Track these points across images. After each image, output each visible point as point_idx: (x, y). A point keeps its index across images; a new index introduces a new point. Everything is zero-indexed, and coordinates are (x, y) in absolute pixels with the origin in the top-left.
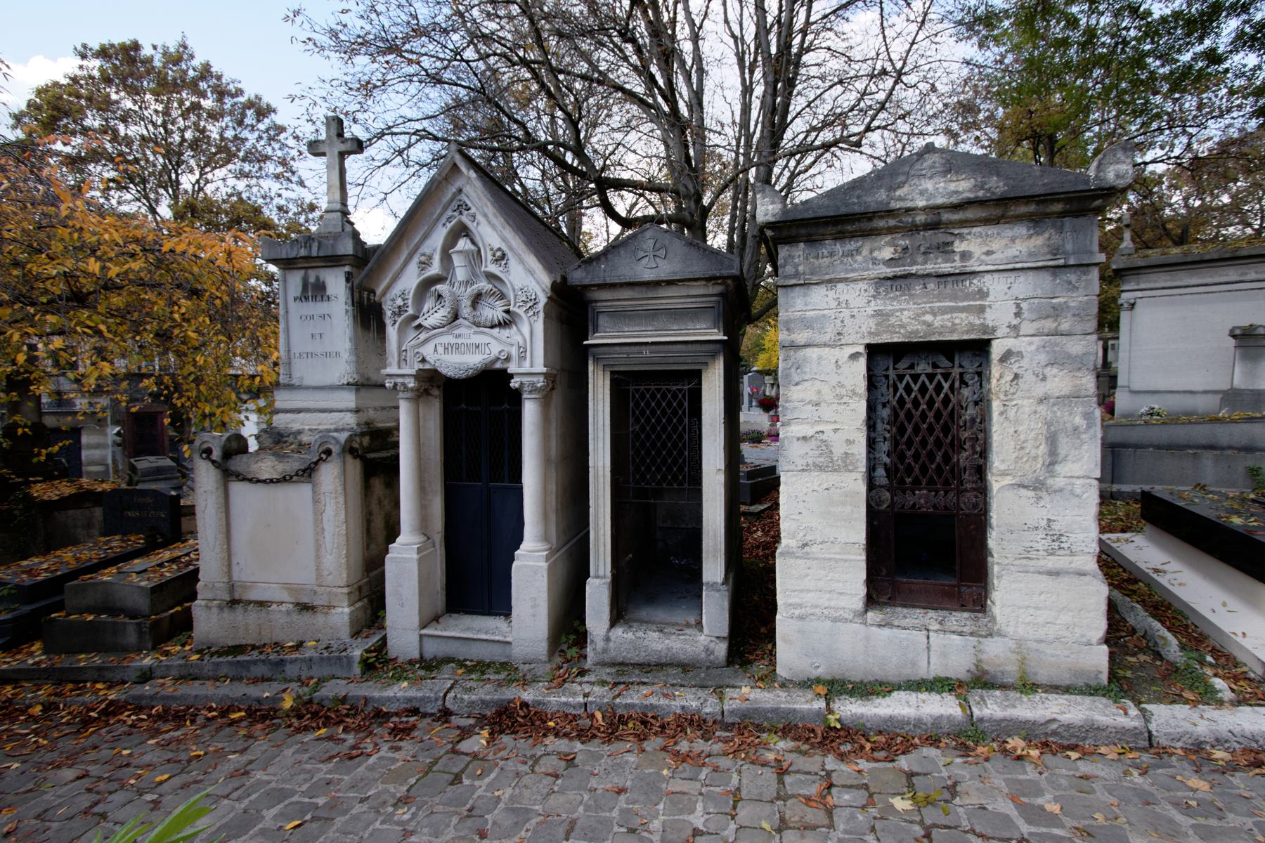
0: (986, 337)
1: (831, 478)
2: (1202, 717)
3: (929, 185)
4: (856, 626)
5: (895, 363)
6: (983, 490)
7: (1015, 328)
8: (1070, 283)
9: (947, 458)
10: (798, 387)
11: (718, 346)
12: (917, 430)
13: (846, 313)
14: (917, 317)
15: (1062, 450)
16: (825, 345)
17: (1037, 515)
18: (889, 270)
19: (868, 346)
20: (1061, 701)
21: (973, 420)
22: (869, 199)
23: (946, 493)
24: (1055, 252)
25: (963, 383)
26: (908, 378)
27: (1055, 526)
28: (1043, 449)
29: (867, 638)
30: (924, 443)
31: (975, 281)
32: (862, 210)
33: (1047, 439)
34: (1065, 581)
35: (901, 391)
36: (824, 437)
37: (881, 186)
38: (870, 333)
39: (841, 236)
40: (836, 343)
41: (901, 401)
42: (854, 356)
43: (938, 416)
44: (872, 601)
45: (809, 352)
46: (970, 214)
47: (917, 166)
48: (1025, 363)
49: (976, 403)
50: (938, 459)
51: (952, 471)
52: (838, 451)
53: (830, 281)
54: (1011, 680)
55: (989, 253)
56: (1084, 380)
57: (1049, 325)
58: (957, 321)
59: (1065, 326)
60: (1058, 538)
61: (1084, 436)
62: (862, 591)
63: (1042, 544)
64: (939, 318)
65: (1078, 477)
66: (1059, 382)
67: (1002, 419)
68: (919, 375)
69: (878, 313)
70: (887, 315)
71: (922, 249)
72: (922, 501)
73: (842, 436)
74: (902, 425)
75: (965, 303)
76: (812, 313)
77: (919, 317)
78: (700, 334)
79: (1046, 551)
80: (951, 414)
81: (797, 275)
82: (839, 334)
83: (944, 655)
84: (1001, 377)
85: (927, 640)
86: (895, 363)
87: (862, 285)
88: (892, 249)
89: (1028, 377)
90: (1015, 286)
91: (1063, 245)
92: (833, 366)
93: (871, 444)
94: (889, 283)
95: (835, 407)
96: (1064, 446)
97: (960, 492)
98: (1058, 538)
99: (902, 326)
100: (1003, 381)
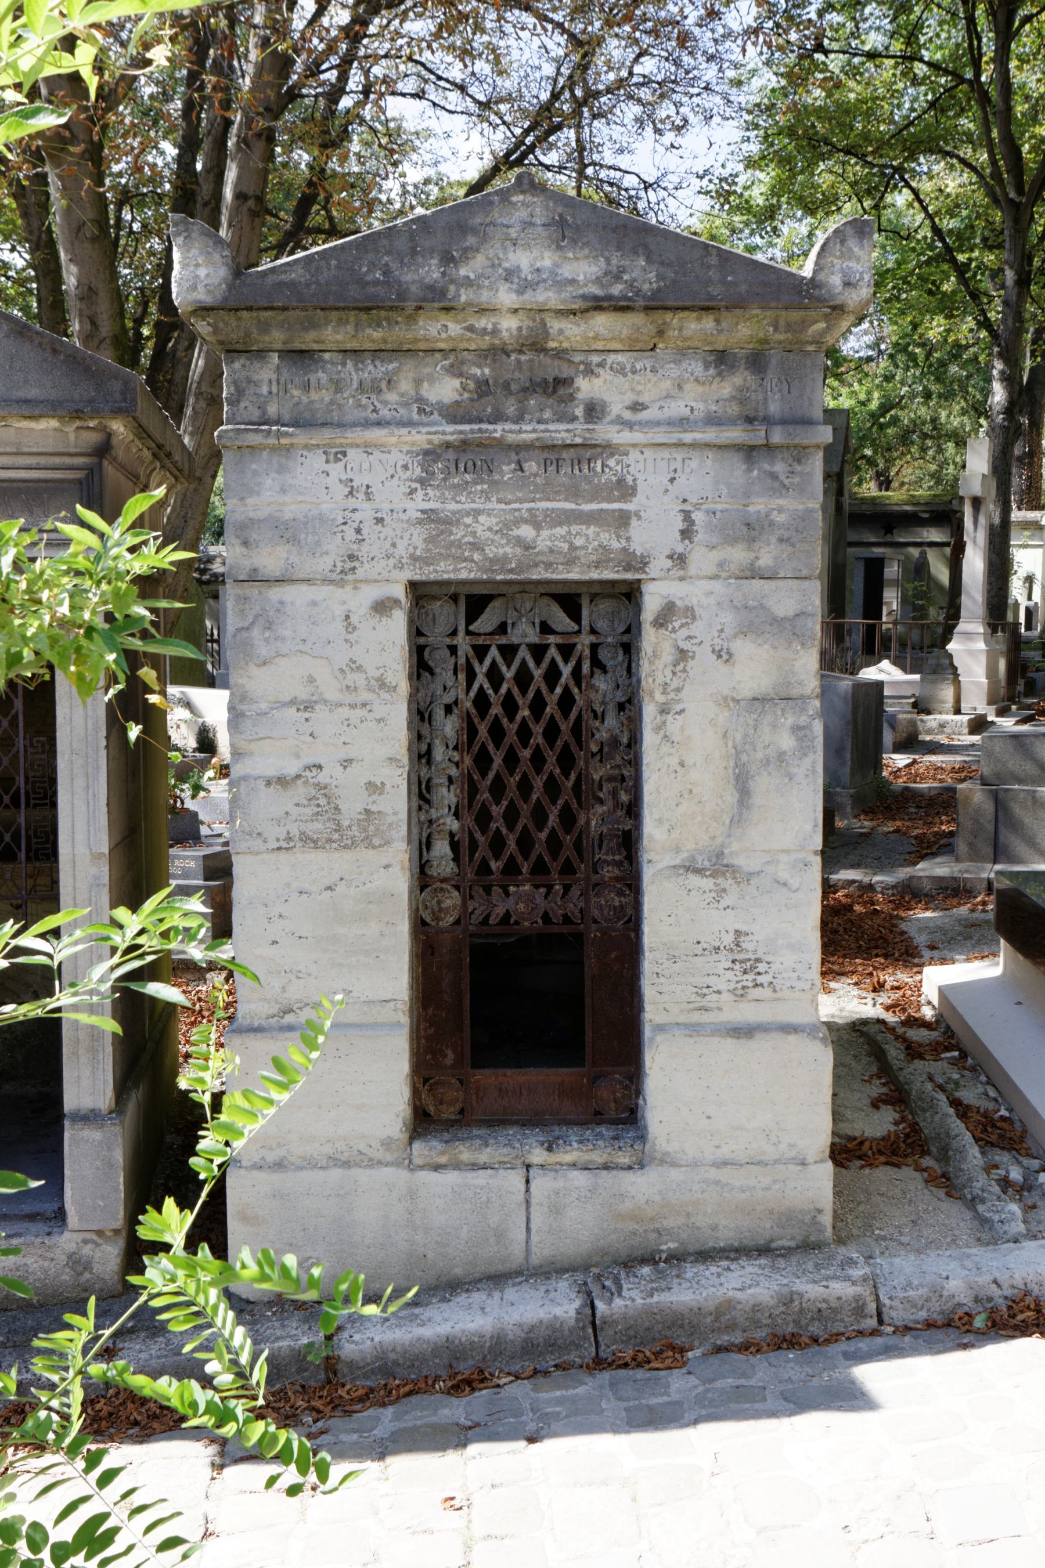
0: (629, 576)
4: (401, 1176)
6: (631, 884)
7: (680, 560)
8: (774, 476)
9: (568, 818)
12: (511, 760)
14: (505, 527)
17: (718, 924)
19: (413, 586)
20: (750, 1269)
21: (615, 742)
25: (597, 664)
26: (494, 653)
29: (412, 1194)
31: (611, 462)
34: (761, 1044)
35: (481, 680)
36: (323, 777)
40: (345, 574)
41: (482, 702)
42: (382, 607)
43: (552, 732)
44: (423, 1121)
48: (697, 629)
49: (621, 707)
50: (553, 820)
51: (578, 846)
52: (352, 806)
57: (738, 555)
58: (579, 542)
59: (765, 560)
63: (725, 980)
64: (545, 533)
66: (755, 667)
69: (429, 517)
73: (359, 774)
74: (483, 752)
75: (594, 506)
77: (510, 531)
79: (733, 991)
80: (577, 729)
83: (556, 1210)
86: (470, 620)
88: (456, 383)
89: (704, 656)
90: (682, 480)
92: (340, 625)
93: (422, 793)
95: (344, 712)
96: (763, 784)
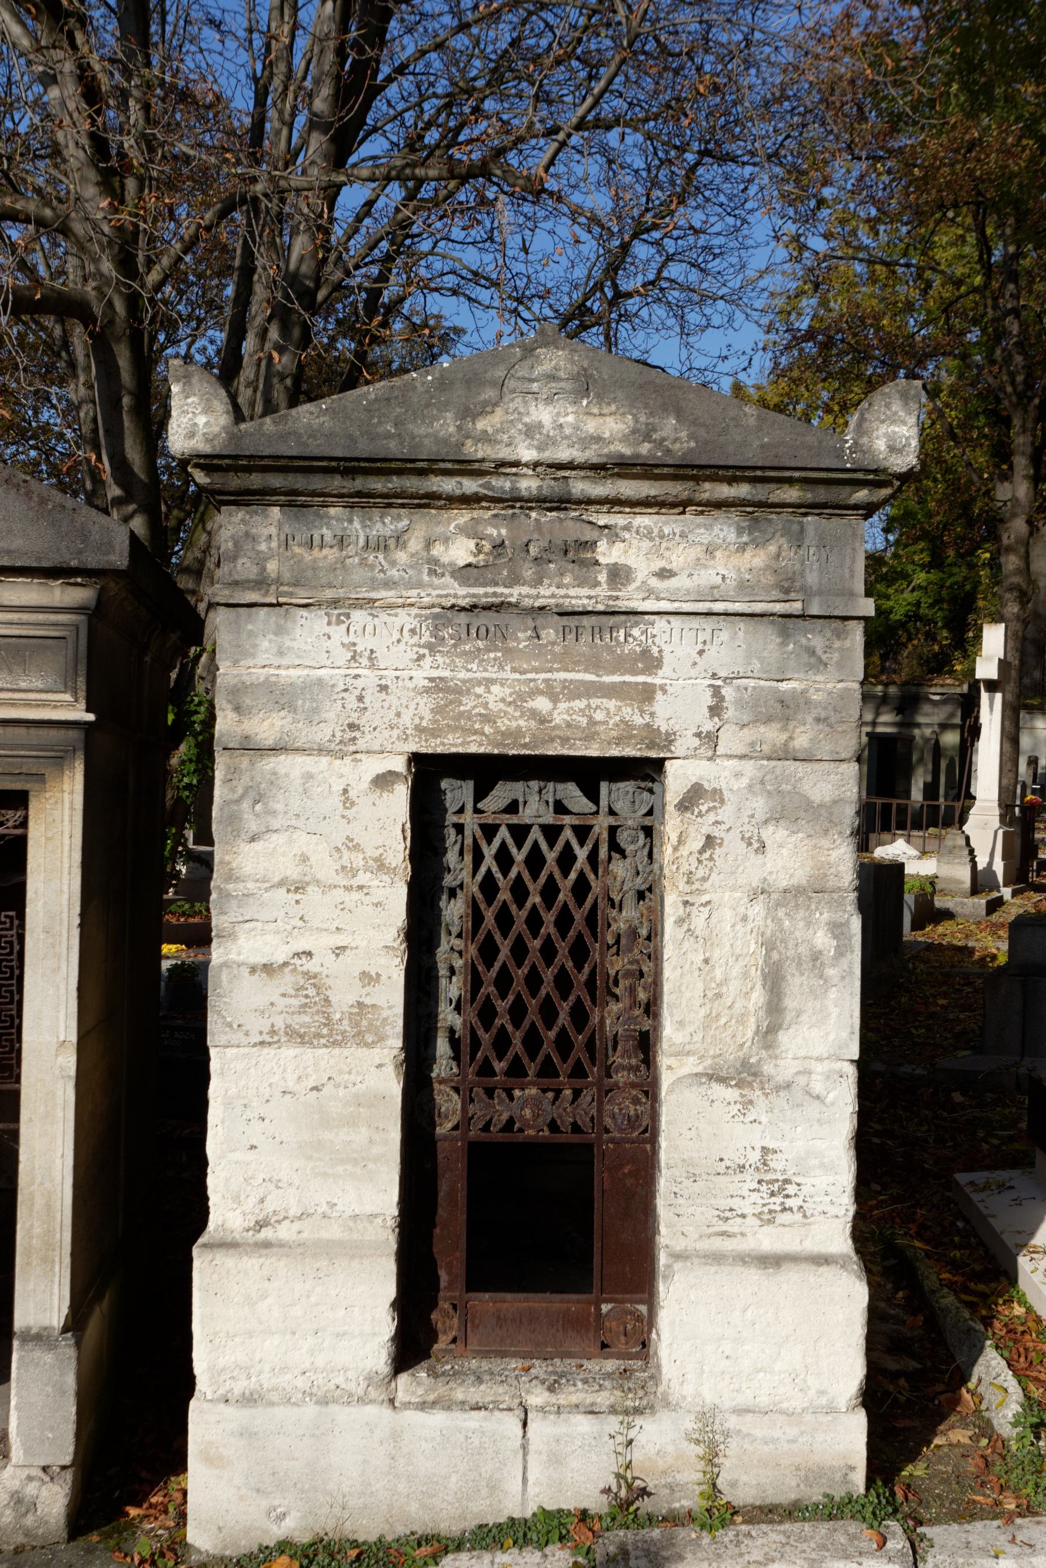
0: (653, 754)
1: (320, 1061)
2: (1013, 1541)
3: (543, 414)
5: (480, 794)
7: (711, 739)
8: (812, 652)
10: (258, 846)
11: (73, 734)
12: (519, 951)
13: (369, 679)
15: (790, 1003)
16: (321, 751)
17: (742, 1139)
18: (462, 591)
22: (422, 430)
23: (577, 1093)
24: (787, 585)
25: (615, 847)
26: (503, 833)
27: (777, 1163)
28: (758, 997)
29: (395, 1436)
30: (534, 981)
31: (636, 632)
32: (405, 452)
33: (765, 977)
34: (791, 1277)
35: (489, 862)
37: (445, 406)
38: (420, 730)
39: (361, 501)
40: (347, 744)
42: (383, 781)
43: (564, 921)
44: (411, 1347)
45: (282, 763)
46: (628, 488)
47: (522, 371)
48: (726, 813)
50: (563, 1018)
52: (344, 996)
53: (335, 603)
54: (686, 1503)
55: (664, 574)
56: (834, 855)
57: (772, 735)
58: (599, 716)
59: (801, 741)
60: (780, 1187)
61: (830, 972)
62: (383, 1327)
64: (562, 706)
65: (819, 1059)
67: (680, 933)
68: (528, 828)
69: (437, 685)
70: (457, 691)
71: (533, 550)
72: (527, 1113)
73: (353, 963)
75: (616, 678)
76: (292, 672)
77: (516, 701)
78: (28, 704)
79: (758, 1216)
80: (591, 919)
81: (261, 583)
82: (352, 726)
83: (556, 1459)
84: (680, 841)
85: (526, 1443)
87: (406, 619)
88: (471, 544)
89: (732, 846)
90: (712, 651)
91: (802, 573)
92: (337, 800)
94: (463, 618)
95: (339, 894)
97: (606, 1091)
98: (780, 1187)
99: (488, 718)
100: (684, 851)
